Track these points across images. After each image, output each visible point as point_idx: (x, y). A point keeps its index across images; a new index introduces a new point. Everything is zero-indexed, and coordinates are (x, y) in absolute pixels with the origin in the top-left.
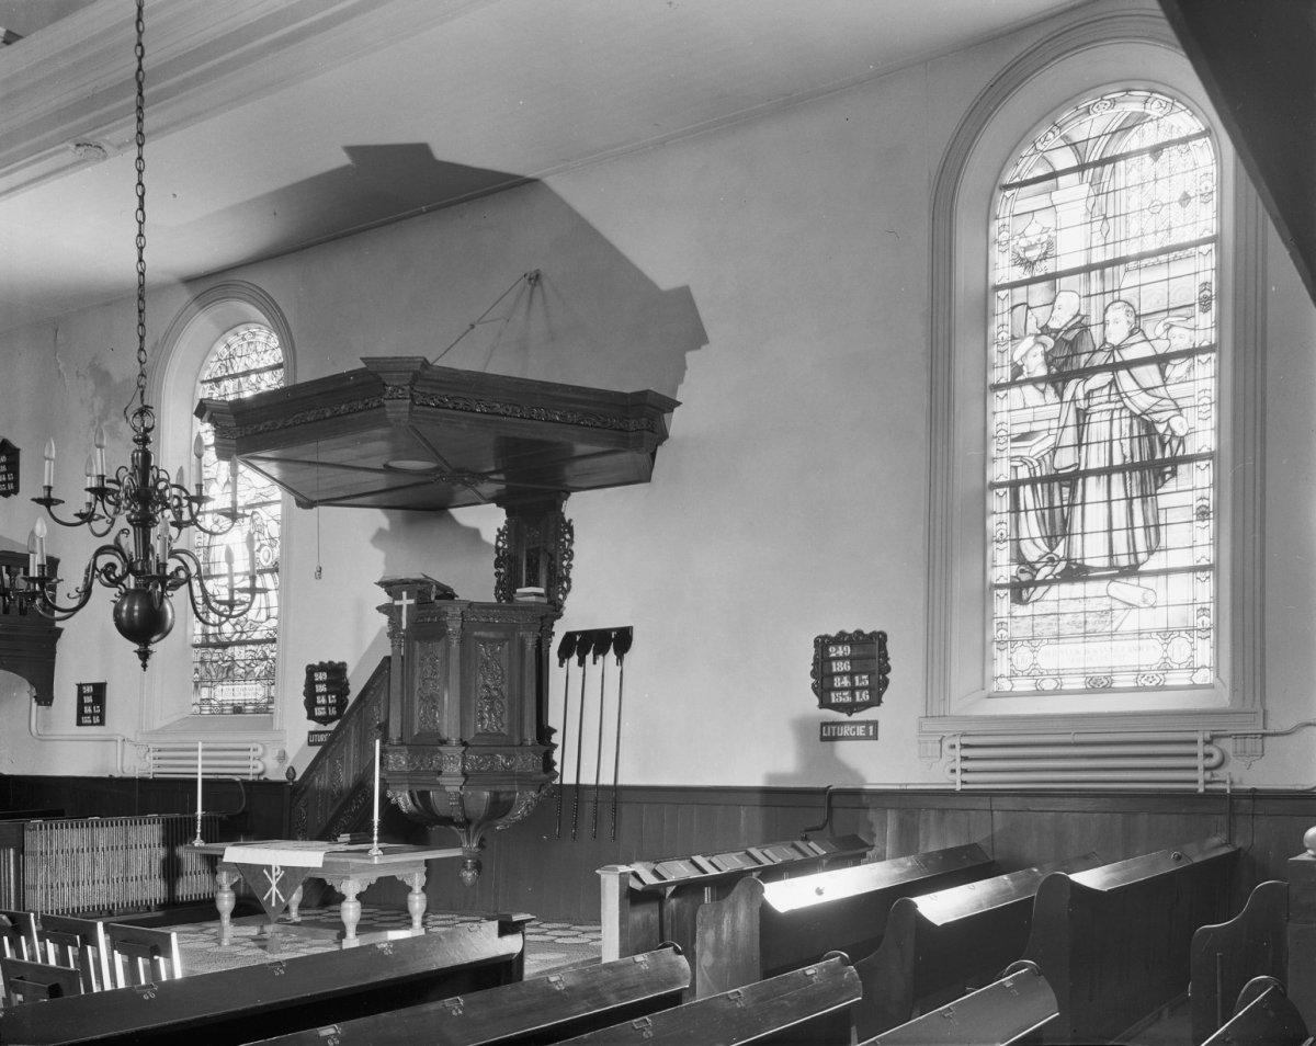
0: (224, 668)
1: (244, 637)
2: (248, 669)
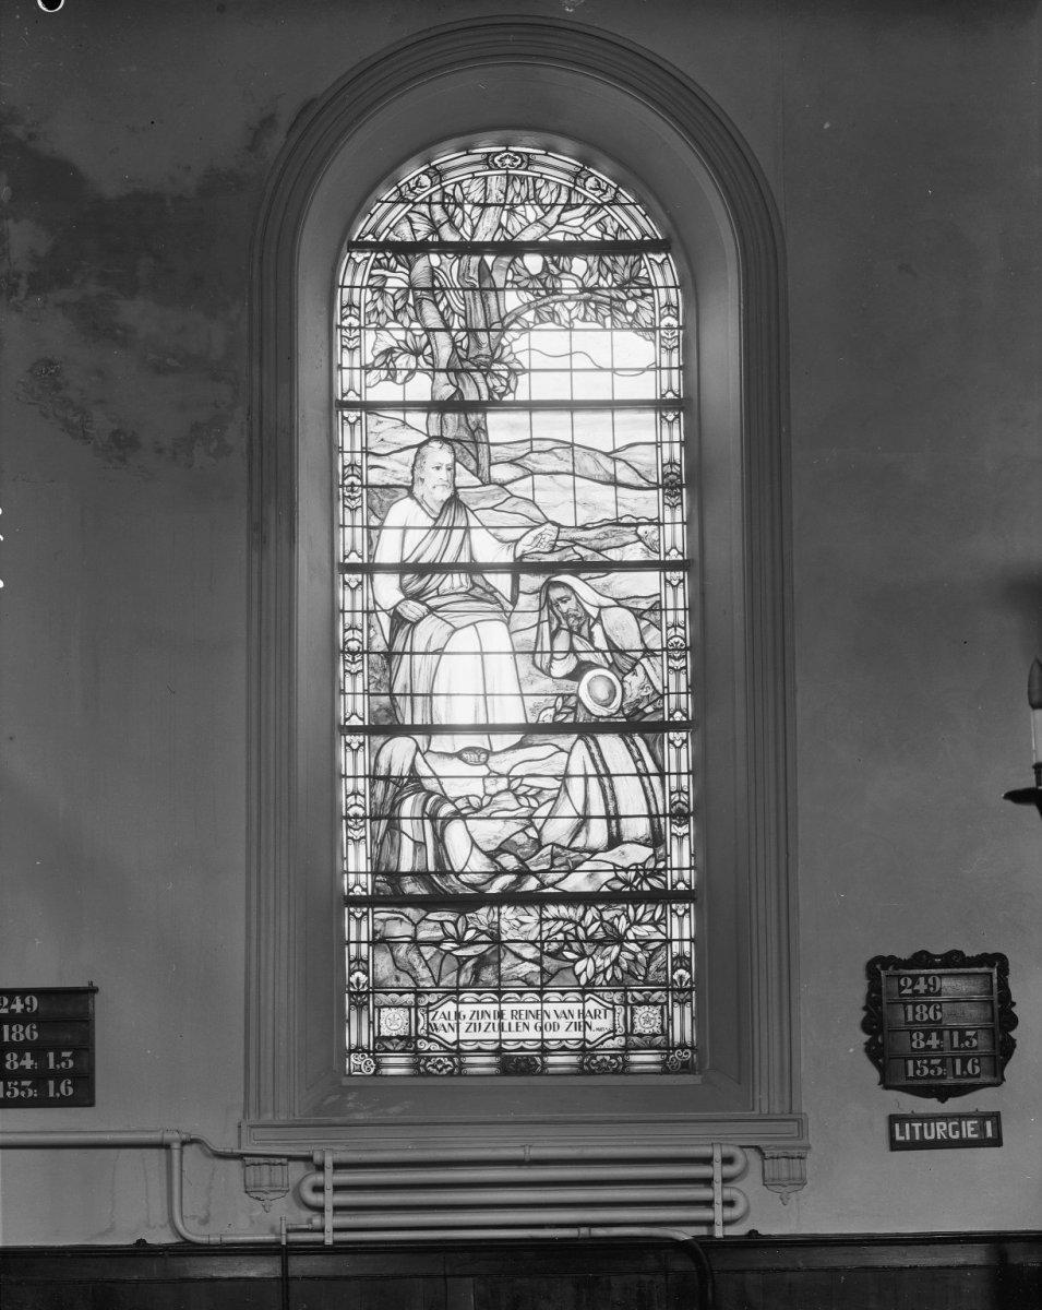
0: (462, 961)
1: (531, 884)
2: (549, 963)
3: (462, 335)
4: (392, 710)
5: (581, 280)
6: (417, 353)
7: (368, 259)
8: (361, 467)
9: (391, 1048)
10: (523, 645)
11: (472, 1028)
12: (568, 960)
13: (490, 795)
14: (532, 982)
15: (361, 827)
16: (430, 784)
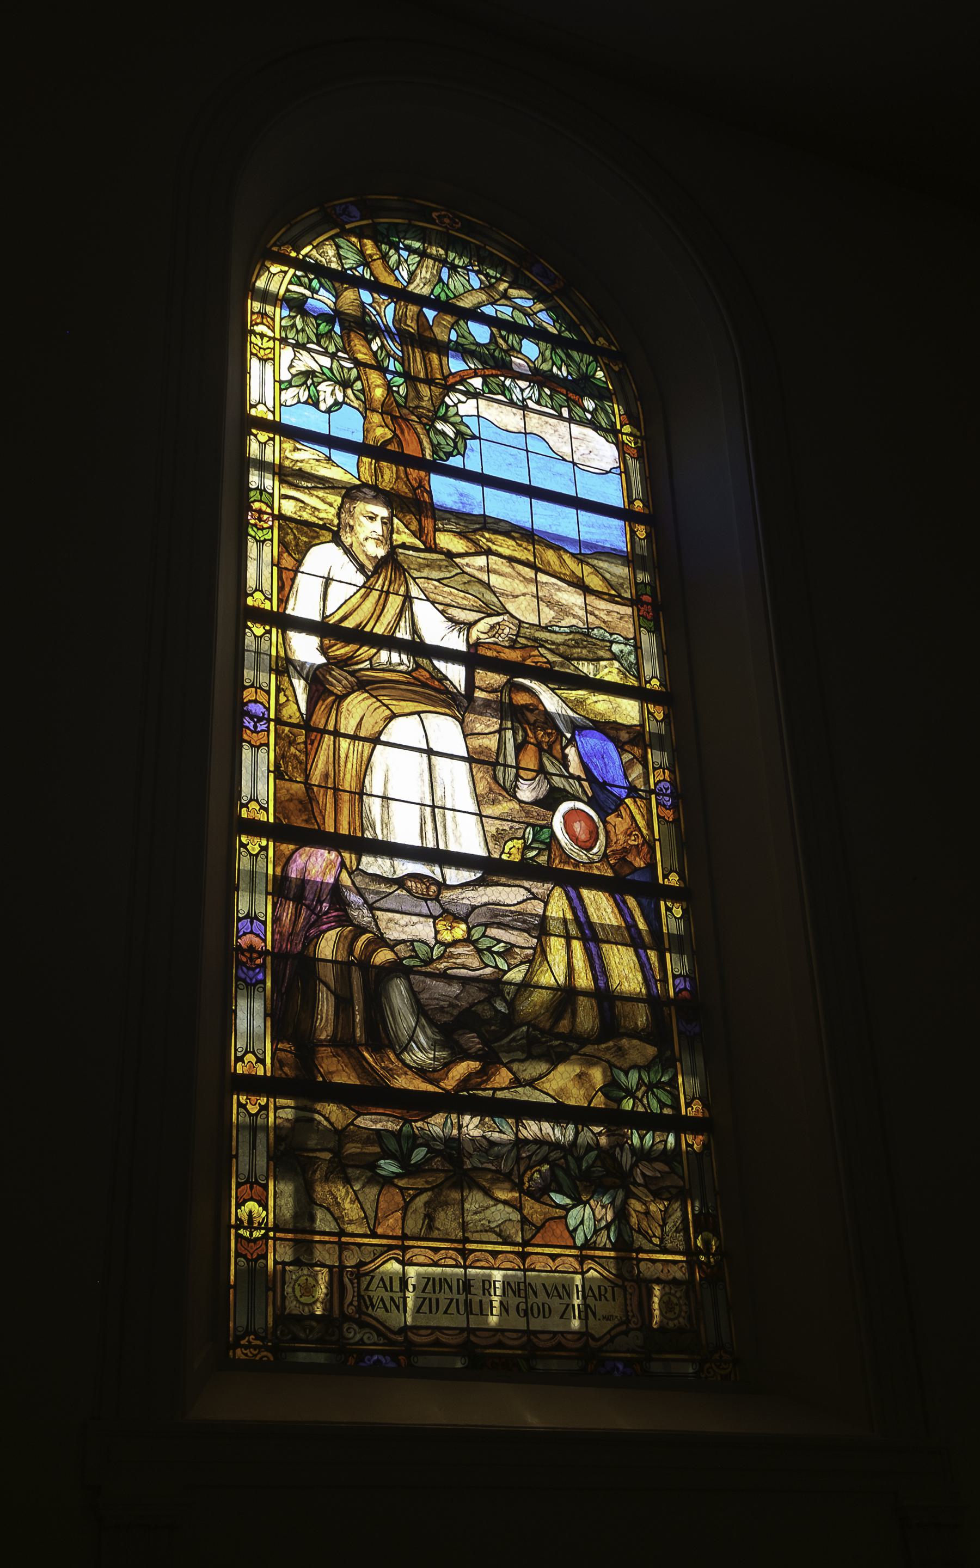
2: (531, 1206)
3: (399, 380)
4: (309, 801)
5: (534, 363)
6: (345, 384)
7: (286, 273)
8: (272, 495)
9: (302, 1335)
10: (482, 753)
11: (425, 1308)
12: (558, 1206)
13: (442, 944)
14: (509, 1236)
15: (258, 966)
16: (362, 916)
